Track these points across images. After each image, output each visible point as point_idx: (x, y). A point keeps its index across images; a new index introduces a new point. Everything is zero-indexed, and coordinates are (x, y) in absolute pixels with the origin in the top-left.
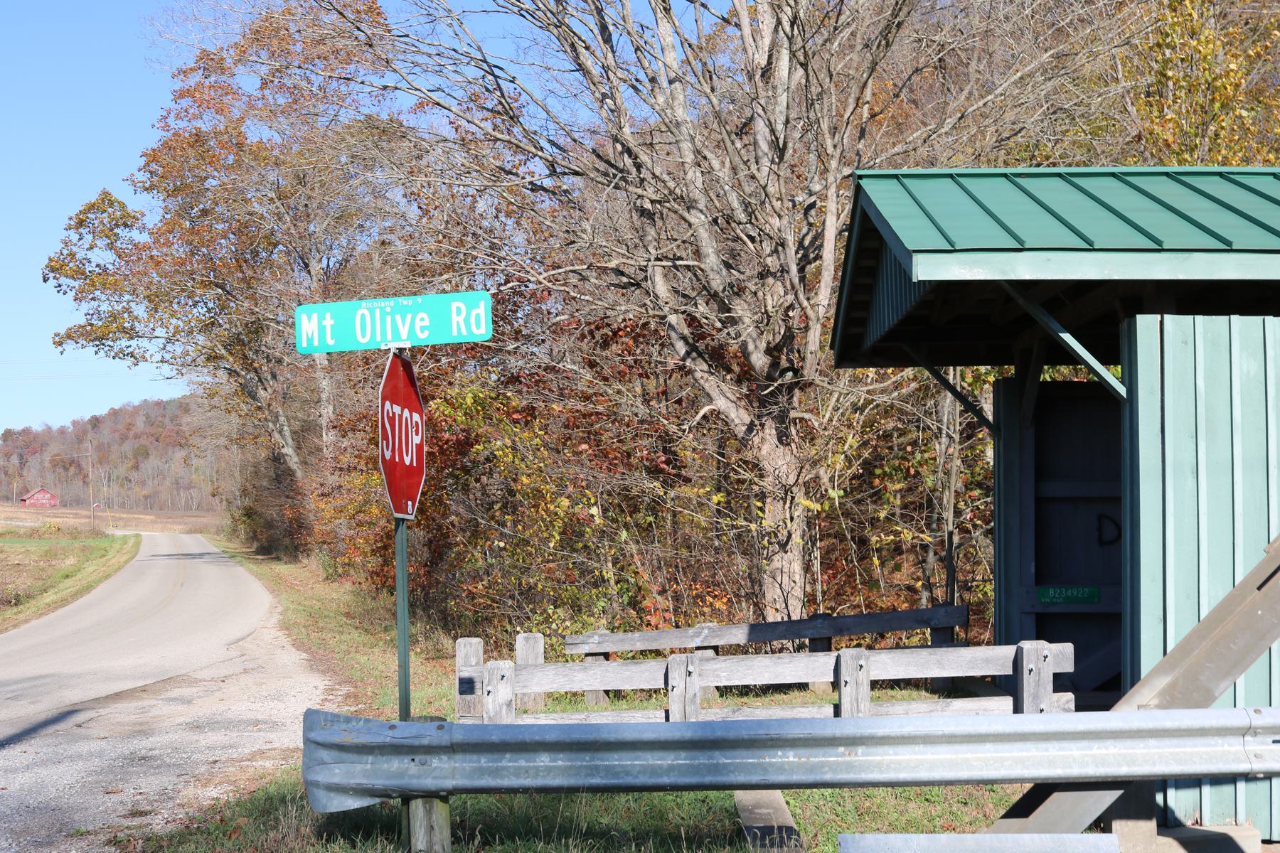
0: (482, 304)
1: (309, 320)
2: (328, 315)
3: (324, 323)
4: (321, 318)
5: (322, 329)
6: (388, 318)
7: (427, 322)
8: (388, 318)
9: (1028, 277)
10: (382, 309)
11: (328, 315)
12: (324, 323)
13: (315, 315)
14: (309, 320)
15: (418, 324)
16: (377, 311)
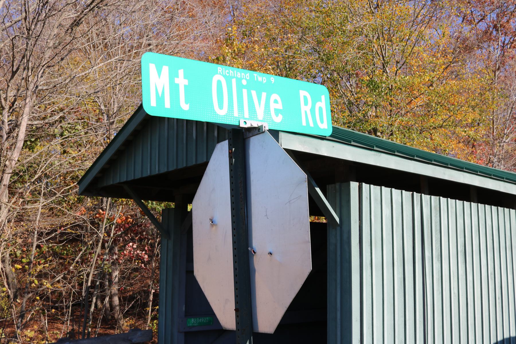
0: (323, 97)
1: (159, 73)
2: (181, 72)
3: (177, 81)
4: (173, 75)
5: (174, 88)
6: (245, 91)
7: (279, 106)
8: (245, 91)
9: (326, 155)
10: (239, 81)
11: (181, 72)
12: (177, 81)
13: (165, 69)
14: (159, 73)
15: (273, 106)
16: (234, 81)
